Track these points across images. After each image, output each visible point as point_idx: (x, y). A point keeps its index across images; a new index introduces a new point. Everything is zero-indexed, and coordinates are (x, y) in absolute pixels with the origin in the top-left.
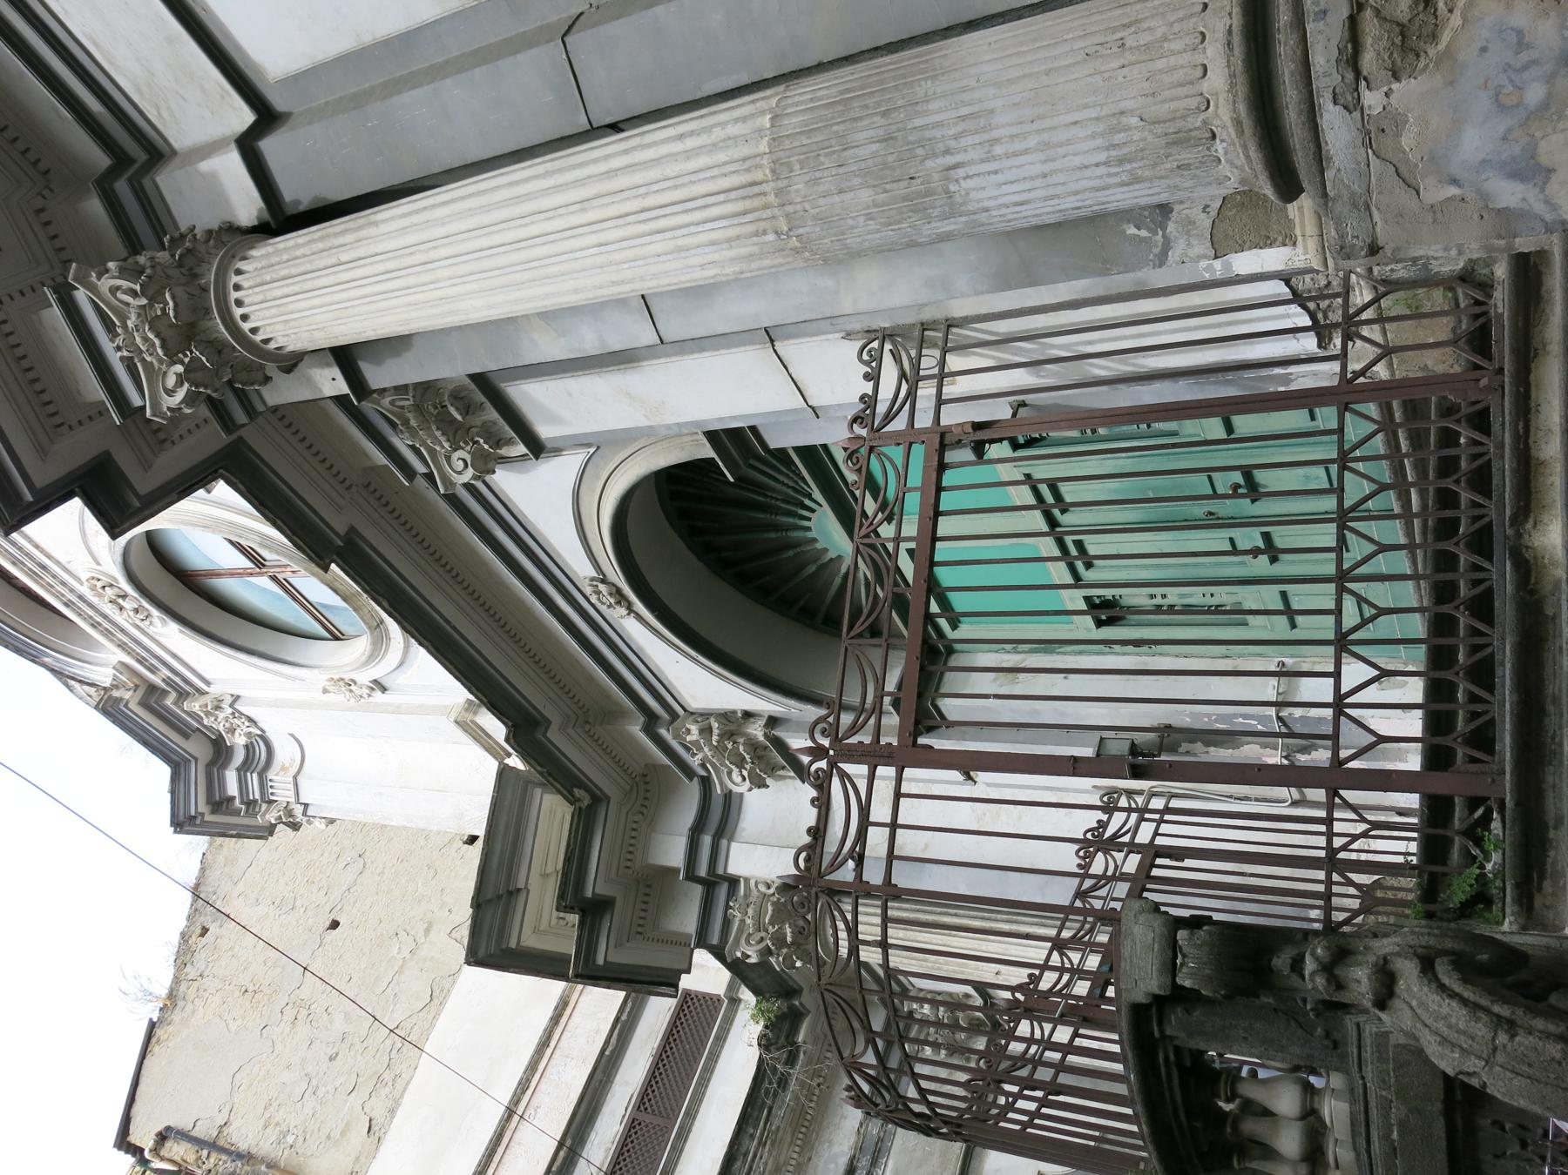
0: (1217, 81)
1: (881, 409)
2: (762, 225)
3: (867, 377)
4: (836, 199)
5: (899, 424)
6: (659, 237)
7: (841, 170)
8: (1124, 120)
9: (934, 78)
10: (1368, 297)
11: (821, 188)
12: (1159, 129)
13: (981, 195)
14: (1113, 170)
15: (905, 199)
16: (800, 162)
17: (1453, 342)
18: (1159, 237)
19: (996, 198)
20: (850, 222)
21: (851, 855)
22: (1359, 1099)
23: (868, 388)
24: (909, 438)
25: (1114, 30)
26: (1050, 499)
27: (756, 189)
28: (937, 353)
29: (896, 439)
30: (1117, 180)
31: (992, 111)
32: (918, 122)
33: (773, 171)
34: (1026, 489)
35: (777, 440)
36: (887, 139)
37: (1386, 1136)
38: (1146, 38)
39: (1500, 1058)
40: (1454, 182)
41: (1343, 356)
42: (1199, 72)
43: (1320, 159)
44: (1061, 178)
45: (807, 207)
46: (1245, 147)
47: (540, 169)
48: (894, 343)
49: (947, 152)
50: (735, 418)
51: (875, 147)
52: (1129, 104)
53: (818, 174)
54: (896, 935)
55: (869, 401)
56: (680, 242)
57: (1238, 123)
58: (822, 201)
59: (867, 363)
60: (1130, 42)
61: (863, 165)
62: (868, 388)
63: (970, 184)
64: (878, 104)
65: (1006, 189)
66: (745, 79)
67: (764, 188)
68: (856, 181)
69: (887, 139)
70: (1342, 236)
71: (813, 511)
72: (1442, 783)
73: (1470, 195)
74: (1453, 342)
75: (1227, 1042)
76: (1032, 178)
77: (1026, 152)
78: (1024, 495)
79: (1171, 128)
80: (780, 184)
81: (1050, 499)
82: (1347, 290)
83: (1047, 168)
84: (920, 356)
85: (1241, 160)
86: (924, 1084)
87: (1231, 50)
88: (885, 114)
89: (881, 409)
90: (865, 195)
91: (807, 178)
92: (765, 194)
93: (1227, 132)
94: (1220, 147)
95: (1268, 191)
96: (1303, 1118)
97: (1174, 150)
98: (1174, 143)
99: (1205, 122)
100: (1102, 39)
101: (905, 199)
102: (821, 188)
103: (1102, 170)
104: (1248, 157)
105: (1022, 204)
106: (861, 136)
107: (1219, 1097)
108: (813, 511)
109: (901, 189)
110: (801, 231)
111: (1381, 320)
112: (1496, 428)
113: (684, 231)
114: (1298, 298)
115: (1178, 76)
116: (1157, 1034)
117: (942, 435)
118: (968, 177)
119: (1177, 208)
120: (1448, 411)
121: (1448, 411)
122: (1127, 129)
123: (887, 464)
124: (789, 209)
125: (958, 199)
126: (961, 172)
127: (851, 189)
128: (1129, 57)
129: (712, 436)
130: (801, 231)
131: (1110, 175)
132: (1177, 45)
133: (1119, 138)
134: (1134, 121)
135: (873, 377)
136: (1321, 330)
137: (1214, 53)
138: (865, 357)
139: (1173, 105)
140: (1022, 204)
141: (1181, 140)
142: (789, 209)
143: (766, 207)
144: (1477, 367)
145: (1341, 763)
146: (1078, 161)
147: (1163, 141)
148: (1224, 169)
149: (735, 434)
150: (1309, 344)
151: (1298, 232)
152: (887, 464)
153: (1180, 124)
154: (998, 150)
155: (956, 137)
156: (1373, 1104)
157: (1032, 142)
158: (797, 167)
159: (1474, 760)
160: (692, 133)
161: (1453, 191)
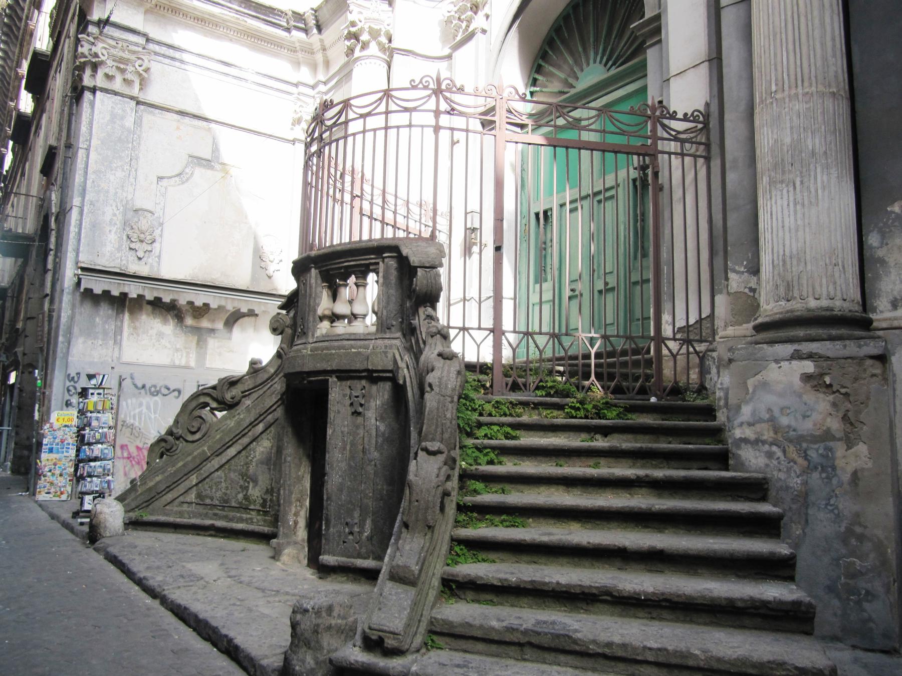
0: (813, 304)
1: (666, 122)
2: (780, 84)
3: (686, 115)
4: (788, 125)
5: (661, 132)
6: (783, 25)
7: (802, 129)
8: (803, 264)
9: (838, 177)
10: (697, 349)
11: (794, 118)
12: (795, 279)
13: (779, 197)
14: (780, 257)
15: (783, 160)
16: (809, 108)
17: (676, 382)
18: (742, 269)
19: (776, 203)
20: (775, 131)
21: (453, 109)
22: (365, 338)
23: (680, 115)
24: (655, 138)
25: (843, 262)
26: (608, 194)
27: (799, 83)
28: (692, 151)
29: (654, 130)
30: (775, 259)
31: (817, 205)
32: (819, 170)
33: (807, 93)
34: (613, 183)
35: (651, 55)
36: (813, 153)
37: (352, 347)
38: (837, 275)
39: (442, 398)
40: (754, 391)
41: (674, 339)
42: (817, 296)
43: (772, 342)
44: (781, 234)
45: (786, 110)
46: (781, 313)
47: (837, 32)
48: (701, 129)
49: (802, 182)
50: (667, 33)
51: (810, 147)
52: (809, 267)
53: (802, 117)
54: (416, 131)
55: (673, 116)
56: (778, 36)
57: (792, 311)
58: (788, 118)
59: (692, 114)
60: (836, 268)
61: (803, 141)
62: (680, 115)
63: (785, 191)
64: (831, 150)
65: (779, 209)
66: (856, 69)
67: (800, 87)
68: (795, 137)
69: (813, 153)
70: (738, 349)
71: (605, 65)
72: (498, 372)
73: (748, 397)
74: (676, 382)
75: (384, 284)
76: (783, 222)
77: (796, 220)
78: (610, 182)
79: (795, 283)
80: (800, 97)
81: (608, 194)
82: (701, 341)
83: (786, 228)
84: (692, 143)
85: (775, 310)
86: (341, 142)
87: (827, 310)
88: (825, 153)
89: (666, 122)
90: (788, 140)
91: (801, 111)
92: (797, 87)
93: (789, 306)
94: (783, 303)
95: (760, 320)
96: (353, 314)
97: (785, 284)
98: (788, 285)
99: (795, 298)
100: (840, 256)
101: (783, 160)
102: (794, 118)
103: (781, 253)
104: (776, 314)
105: (771, 214)
106: (817, 141)
107: (356, 278)
108: (605, 65)
109: (788, 159)
110: (775, 105)
111: (688, 353)
112: (639, 397)
113: (784, 40)
114: (701, 320)
115: (818, 288)
116: (385, 255)
117: (654, 155)
118: (788, 192)
119: (755, 278)
120: (648, 377)
121: (648, 377)
122: (798, 265)
123: (640, 127)
124: (787, 100)
125: (779, 186)
126: (791, 189)
127: (792, 133)
128: (830, 267)
129: (658, 18)
130: (775, 105)
131: (778, 256)
132: (831, 288)
133: (795, 262)
134: (801, 268)
135: (685, 118)
136: (687, 328)
137: (824, 303)
138: (696, 113)
139: (805, 286)
140: (771, 214)
141: (789, 287)
142: (787, 100)
143: (790, 87)
144: (664, 390)
145: (503, 334)
146: (787, 243)
147: (790, 279)
148: (772, 305)
149: (658, 31)
150: (680, 323)
151: (736, 327)
152: (640, 127)
153: (796, 288)
154: (799, 207)
155: (808, 188)
156: (367, 342)
157: (800, 222)
158: (808, 106)
159: (507, 385)
160: (834, 46)
161: (751, 390)
